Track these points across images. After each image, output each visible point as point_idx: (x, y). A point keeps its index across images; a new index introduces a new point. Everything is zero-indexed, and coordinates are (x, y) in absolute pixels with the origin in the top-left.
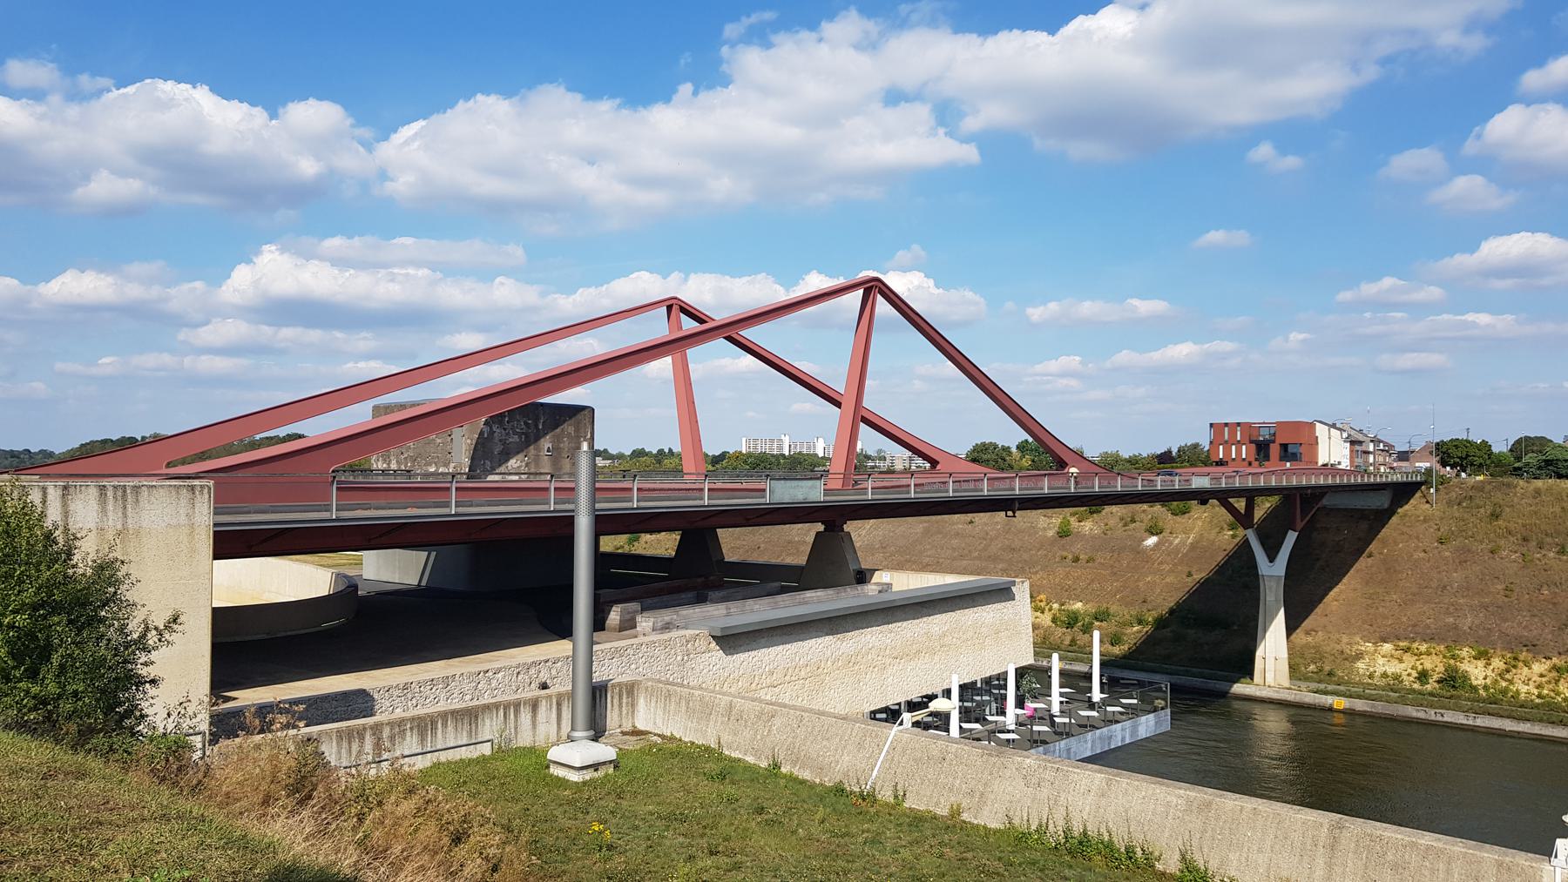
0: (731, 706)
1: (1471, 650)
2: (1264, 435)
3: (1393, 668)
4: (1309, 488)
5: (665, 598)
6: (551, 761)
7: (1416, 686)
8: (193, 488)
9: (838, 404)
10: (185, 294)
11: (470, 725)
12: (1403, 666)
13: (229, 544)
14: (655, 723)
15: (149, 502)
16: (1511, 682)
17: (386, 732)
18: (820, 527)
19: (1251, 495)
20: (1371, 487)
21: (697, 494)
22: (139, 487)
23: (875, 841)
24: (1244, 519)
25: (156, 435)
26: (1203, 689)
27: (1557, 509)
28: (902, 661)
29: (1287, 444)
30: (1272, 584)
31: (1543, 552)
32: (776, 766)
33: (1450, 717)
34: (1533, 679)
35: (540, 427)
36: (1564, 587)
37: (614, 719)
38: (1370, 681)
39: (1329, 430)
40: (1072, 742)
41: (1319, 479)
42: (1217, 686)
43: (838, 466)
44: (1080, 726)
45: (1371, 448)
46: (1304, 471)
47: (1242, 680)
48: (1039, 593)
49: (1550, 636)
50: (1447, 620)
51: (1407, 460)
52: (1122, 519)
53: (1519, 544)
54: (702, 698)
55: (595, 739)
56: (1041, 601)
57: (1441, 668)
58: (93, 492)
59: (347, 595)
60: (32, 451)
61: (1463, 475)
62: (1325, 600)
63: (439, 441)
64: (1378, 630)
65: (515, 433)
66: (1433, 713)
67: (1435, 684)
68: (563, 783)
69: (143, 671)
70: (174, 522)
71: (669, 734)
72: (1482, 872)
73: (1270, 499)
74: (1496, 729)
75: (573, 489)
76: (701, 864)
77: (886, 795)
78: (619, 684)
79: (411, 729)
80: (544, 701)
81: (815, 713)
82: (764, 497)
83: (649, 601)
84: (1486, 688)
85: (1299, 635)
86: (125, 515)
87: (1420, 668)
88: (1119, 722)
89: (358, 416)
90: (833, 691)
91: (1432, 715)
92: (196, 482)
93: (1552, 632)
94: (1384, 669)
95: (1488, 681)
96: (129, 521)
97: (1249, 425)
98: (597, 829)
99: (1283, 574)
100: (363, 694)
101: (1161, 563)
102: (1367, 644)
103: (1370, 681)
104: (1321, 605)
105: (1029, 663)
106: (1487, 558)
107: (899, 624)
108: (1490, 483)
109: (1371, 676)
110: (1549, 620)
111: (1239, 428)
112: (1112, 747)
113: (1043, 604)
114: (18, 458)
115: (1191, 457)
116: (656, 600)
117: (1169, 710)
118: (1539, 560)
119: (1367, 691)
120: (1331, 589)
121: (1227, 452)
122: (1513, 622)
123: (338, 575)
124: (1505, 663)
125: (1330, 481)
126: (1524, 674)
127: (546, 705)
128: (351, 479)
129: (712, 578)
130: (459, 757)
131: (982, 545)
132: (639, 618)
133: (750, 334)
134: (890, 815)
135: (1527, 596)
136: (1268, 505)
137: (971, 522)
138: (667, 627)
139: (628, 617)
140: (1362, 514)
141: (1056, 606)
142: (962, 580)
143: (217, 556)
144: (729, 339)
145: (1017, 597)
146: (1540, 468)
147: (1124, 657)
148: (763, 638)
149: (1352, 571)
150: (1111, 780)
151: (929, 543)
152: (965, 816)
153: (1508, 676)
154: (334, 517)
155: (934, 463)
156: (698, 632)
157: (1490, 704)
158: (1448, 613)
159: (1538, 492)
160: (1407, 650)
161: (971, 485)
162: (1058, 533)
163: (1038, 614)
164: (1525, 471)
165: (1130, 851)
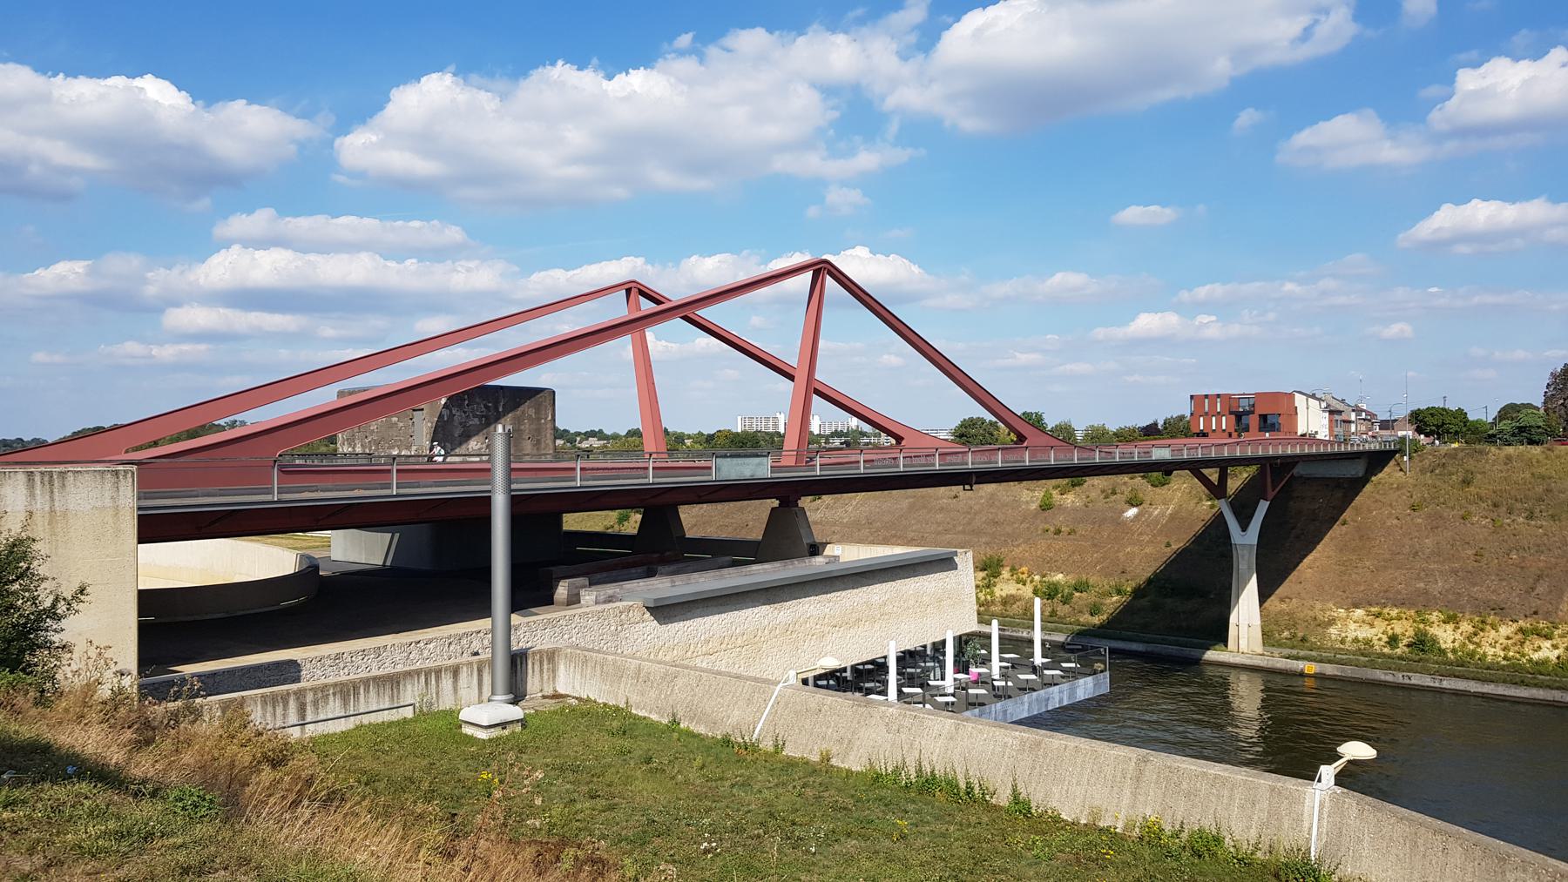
0: (639, 669)
1: (1440, 615)
2: (1244, 406)
3: (1364, 633)
4: (1277, 458)
5: (614, 573)
6: (463, 721)
7: (1386, 650)
8: (117, 473)
9: (791, 378)
10: (159, 280)
11: (392, 690)
12: (1374, 631)
13: (154, 528)
14: (573, 687)
15: (75, 486)
16: (1478, 645)
17: (310, 697)
18: (776, 503)
19: (1224, 465)
20: (1319, 458)
21: (641, 472)
22: (65, 473)
23: (746, 785)
24: (1217, 491)
25: (98, 428)
26: (1178, 657)
27: (1528, 475)
28: (842, 629)
29: (1266, 415)
30: (1245, 552)
31: (1513, 518)
32: (675, 722)
33: (1417, 679)
34: (1500, 642)
35: (501, 410)
36: (1532, 551)
37: (534, 683)
38: (1342, 646)
39: (1307, 400)
40: (1009, 704)
41: (1287, 448)
42: (1192, 653)
43: (791, 443)
44: (1020, 689)
45: (1353, 417)
46: (1289, 441)
47: (1217, 647)
48: (1021, 566)
49: (1517, 599)
50: (1418, 586)
51: (1387, 429)
52: (1103, 491)
53: (1490, 510)
54: (615, 662)
55: (515, 702)
56: (1023, 573)
57: (1411, 632)
58: (21, 478)
59: (310, 574)
60: (25, 440)
61: (1437, 442)
62: (1298, 568)
63: (401, 424)
64: (1350, 596)
65: (475, 416)
66: (1401, 676)
67: (1404, 648)
68: (471, 740)
69: (56, 638)
70: (99, 504)
71: (586, 697)
72: (1258, 796)
73: (1248, 469)
74: (1541, 700)
75: (489, 470)
76: (579, 806)
77: (767, 745)
78: (540, 651)
79: (334, 694)
80: (465, 669)
81: (713, 673)
82: (711, 475)
83: (598, 576)
84: (1454, 651)
85: (1273, 602)
86: (52, 500)
87: (1390, 632)
88: (1057, 684)
89: (324, 397)
90: (770, 658)
91: (1399, 678)
92: (120, 468)
93: (1519, 596)
94: (1356, 634)
95: (1457, 645)
96: (57, 504)
97: (1229, 397)
98: (485, 777)
99: (1256, 543)
100: (293, 664)
101: (1141, 534)
102: (1339, 610)
103: (1342, 646)
104: (1295, 573)
105: (973, 630)
106: (1458, 524)
107: (838, 594)
108: (1463, 450)
109: (1342, 642)
110: (1517, 584)
111: (1219, 400)
112: (1050, 708)
113: (1024, 576)
114: (11, 447)
115: (1174, 429)
116: (605, 575)
117: (1107, 673)
118: (1509, 525)
119: (1338, 656)
120: (1306, 556)
121: (1208, 423)
122: (1482, 586)
123: (302, 556)
124: (1474, 627)
125: (1298, 451)
126: (1491, 637)
127: (467, 672)
128: (316, 463)
129: (668, 553)
130: (381, 720)
131: (967, 519)
132: (582, 592)
133: (707, 313)
134: (766, 761)
135: (1496, 561)
136: (1245, 475)
137: (956, 497)
138: (610, 600)
139: (575, 591)
140: (1337, 483)
141: (1037, 578)
142: (910, 551)
143: (140, 542)
144: (685, 318)
145: (959, 567)
146: (1513, 435)
147: (1102, 626)
148: (698, 608)
149: (1327, 539)
150: (959, 724)
151: (914, 518)
152: (834, 762)
153: (1475, 639)
154: (276, 499)
155: (899, 439)
156: (632, 603)
157: (1458, 666)
158: (1419, 578)
159: (1509, 458)
160: (1378, 615)
161: (923, 460)
162: (1041, 506)
163: (1020, 586)
164: (1499, 438)
165: (969, 790)
